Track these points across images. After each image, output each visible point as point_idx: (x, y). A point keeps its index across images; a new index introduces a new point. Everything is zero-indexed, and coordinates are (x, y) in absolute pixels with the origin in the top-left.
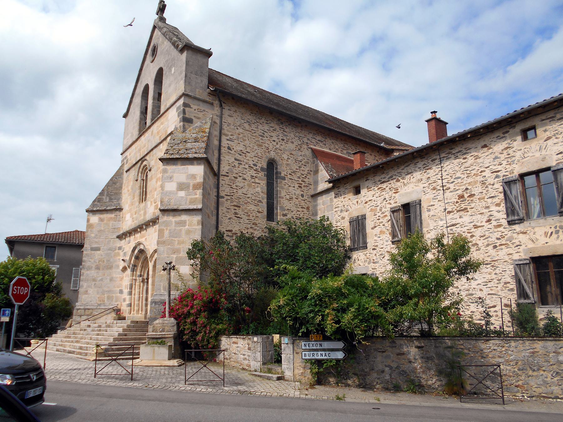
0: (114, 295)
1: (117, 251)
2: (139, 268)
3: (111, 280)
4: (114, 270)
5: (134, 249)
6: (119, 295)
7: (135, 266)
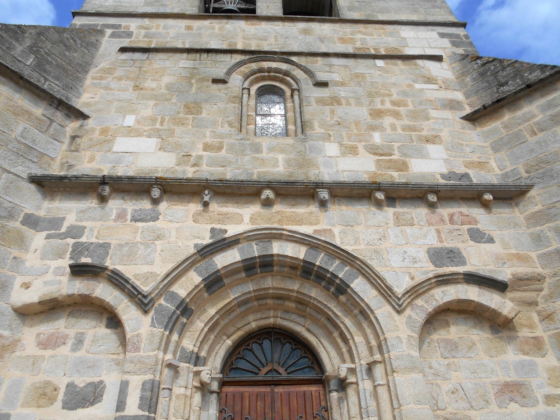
1: (16, 224)
2: (199, 325)
5: (348, 258)
7: (185, 310)
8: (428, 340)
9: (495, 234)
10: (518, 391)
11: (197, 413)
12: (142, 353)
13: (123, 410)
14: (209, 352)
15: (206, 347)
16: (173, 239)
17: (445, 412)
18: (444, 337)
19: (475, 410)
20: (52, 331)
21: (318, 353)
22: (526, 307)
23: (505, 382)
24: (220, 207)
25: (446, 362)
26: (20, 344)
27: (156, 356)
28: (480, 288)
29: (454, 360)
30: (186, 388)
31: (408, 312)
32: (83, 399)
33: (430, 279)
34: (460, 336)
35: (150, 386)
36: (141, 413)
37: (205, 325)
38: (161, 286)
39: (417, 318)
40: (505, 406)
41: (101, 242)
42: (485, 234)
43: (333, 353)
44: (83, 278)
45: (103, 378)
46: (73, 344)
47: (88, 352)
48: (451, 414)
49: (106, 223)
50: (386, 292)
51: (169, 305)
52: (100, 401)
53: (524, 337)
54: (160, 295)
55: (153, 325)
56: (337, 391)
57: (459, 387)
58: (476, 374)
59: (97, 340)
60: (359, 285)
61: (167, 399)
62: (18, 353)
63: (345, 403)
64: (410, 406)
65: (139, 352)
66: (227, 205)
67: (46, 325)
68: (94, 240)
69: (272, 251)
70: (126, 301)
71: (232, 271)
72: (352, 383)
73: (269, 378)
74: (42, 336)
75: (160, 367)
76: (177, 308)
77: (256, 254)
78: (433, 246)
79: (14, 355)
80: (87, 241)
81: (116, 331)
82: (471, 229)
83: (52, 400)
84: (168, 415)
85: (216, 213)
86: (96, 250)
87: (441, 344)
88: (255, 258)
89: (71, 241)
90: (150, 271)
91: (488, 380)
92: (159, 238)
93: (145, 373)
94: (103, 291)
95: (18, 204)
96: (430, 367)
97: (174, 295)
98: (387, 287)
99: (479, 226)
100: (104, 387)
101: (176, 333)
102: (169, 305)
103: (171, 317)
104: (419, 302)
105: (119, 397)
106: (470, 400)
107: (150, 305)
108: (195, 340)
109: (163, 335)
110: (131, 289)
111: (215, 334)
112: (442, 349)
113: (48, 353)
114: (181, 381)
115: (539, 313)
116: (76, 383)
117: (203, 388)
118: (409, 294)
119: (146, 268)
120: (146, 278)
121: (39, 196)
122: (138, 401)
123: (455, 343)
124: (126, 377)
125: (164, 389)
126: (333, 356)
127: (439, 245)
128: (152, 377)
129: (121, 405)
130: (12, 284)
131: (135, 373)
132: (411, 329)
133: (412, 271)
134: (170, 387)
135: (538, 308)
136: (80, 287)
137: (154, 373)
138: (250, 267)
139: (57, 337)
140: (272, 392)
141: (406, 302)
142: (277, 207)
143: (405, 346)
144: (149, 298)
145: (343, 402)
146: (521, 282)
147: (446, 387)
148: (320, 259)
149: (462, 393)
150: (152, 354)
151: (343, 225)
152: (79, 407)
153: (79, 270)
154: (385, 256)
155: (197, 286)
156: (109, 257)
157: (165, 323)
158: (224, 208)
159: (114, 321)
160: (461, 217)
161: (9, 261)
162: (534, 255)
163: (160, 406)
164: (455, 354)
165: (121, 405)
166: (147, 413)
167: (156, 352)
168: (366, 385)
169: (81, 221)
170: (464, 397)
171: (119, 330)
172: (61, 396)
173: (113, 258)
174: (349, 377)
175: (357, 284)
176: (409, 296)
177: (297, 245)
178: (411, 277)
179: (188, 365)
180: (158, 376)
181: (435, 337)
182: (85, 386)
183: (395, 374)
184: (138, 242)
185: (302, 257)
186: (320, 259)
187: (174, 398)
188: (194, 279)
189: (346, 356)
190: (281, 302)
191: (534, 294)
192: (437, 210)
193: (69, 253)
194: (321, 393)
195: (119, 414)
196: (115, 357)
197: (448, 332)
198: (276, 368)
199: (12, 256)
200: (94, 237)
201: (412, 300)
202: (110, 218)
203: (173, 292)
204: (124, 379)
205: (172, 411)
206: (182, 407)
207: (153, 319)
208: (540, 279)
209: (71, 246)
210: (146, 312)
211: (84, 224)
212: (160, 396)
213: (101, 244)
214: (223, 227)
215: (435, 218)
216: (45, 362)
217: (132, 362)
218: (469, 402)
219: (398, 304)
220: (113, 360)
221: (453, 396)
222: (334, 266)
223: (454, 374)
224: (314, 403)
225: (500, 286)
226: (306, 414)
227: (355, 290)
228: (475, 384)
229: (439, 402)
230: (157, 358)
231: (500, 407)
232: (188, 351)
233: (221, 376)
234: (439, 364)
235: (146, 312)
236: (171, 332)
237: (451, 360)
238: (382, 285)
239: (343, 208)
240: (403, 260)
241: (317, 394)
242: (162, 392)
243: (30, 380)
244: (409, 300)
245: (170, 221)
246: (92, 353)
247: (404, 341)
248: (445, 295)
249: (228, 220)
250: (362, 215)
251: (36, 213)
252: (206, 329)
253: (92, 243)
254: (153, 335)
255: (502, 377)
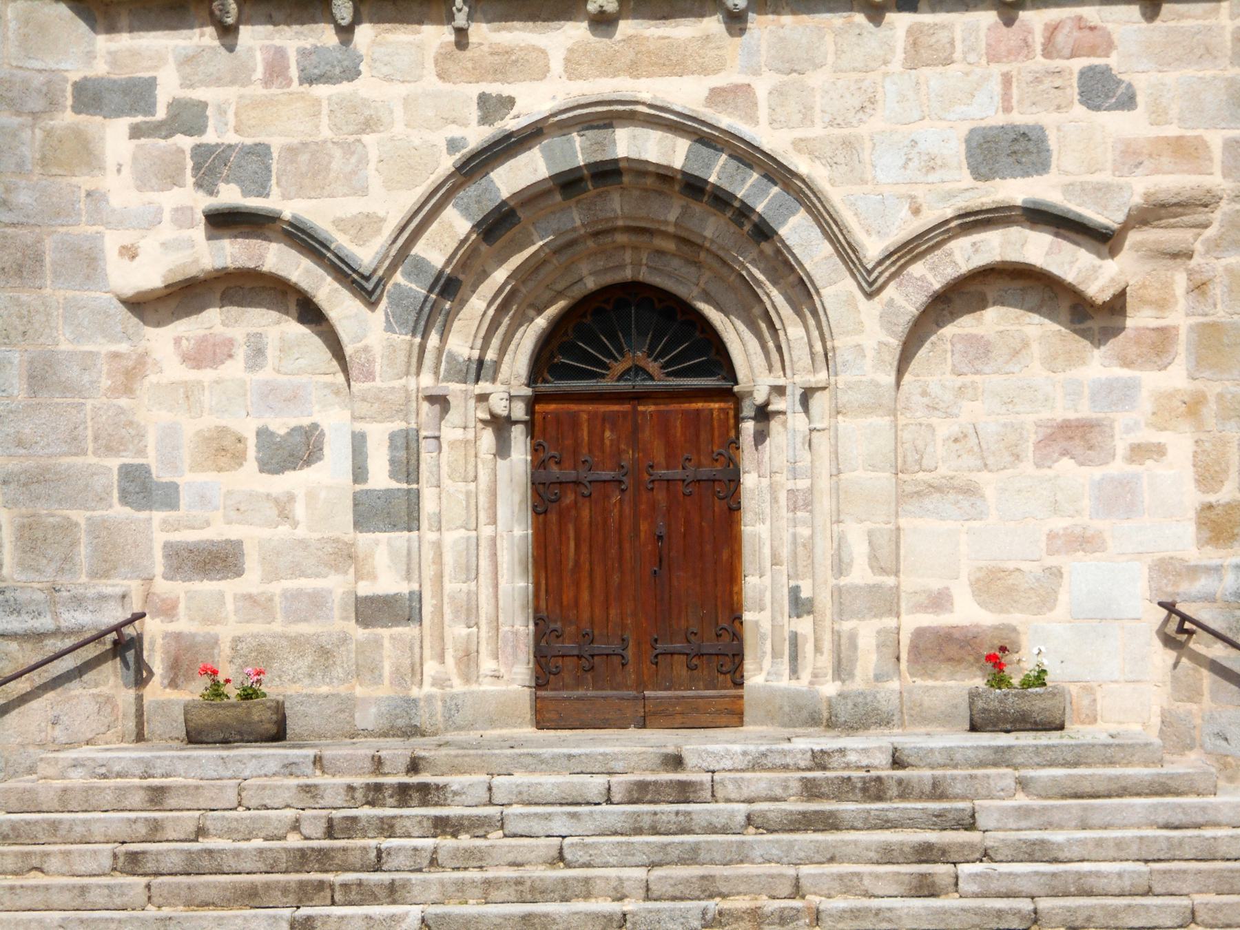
0: (79, 516)
1: (67, 118)
2: (478, 304)
3: (41, 376)
4: (55, 292)
5: (776, 172)
6: (119, 511)
7: (449, 287)
8: (933, 338)
9: (1143, 80)
10: (1083, 437)
11: (491, 465)
12: (378, 383)
13: (365, 480)
14: (502, 351)
15: (495, 342)
16: (399, 128)
17: (933, 474)
18: (967, 330)
19: (990, 471)
20: (201, 332)
22: (1165, 261)
23: (1064, 421)
24: (495, 31)
25: (959, 381)
26: (150, 360)
27: (405, 389)
28: (1057, 235)
29: (977, 378)
30: (465, 428)
31: (890, 291)
32: (292, 455)
33: (946, 222)
34: (1001, 328)
35: (404, 441)
36: (394, 485)
37: (489, 306)
38: (393, 252)
39: (904, 304)
40: (1049, 463)
41: (249, 141)
42: (1119, 82)
44: (235, 232)
45: (316, 418)
46: (248, 356)
47: (279, 372)
48: (944, 477)
49: (247, 91)
50: (847, 252)
51: (414, 286)
52: (319, 459)
53: (1137, 329)
54: (392, 268)
55: (389, 328)
56: (754, 418)
57: (971, 431)
58: (1011, 406)
59: (289, 348)
60: (797, 231)
61: (435, 454)
62: (153, 378)
64: (856, 473)
65: (374, 380)
66: (509, 24)
67: (185, 321)
68: (232, 138)
69: (614, 151)
70: (329, 279)
71: (532, 196)
73: (624, 386)
74: (184, 342)
75: (414, 404)
76: (431, 290)
77: (582, 163)
78: (983, 124)
79: (146, 382)
80: (220, 141)
81: (319, 328)
82: (1092, 68)
83: (239, 459)
84: (439, 480)
85: (485, 48)
86: (243, 163)
87: (959, 346)
88: (579, 168)
89: (185, 142)
90: (365, 211)
91: (1031, 418)
92: (369, 125)
93: (390, 418)
94: (277, 258)
95: (54, 67)
96: (924, 394)
97: (420, 266)
98: (849, 243)
99: (1113, 61)
100: (322, 434)
101: (433, 332)
102: (414, 286)
103: (422, 309)
104: (917, 269)
105: (354, 459)
106: (985, 454)
107: (378, 291)
108: (472, 338)
109: (412, 345)
110: (333, 258)
111: (511, 314)
112: (956, 356)
113: (207, 375)
114: (454, 416)
115: (1190, 273)
116: (271, 428)
117: (500, 425)
118: (895, 257)
119: (363, 207)
120: (364, 225)
121: (82, 27)
122: (386, 467)
123: (988, 343)
124: (360, 426)
125: (425, 438)
127: (1000, 119)
128: (403, 425)
129: (360, 473)
130: (102, 250)
131: (373, 419)
132: (888, 330)
133: (920, 192)
134: (437, 434)
135: (1193, 263)
136: (232, 252)
137: (406, 419)
138: (568, 184)
139: (214, 345)
140: (635, 411)
141: (887, 274)
142: (626, 27)
143: (868, 363)
144: (375, 279)
146: (1163, 211)
147: (945, 428)
148: (717, 168)
149: (973, 441)
150: (397, 383)
151: (779, 71)
152: (288, 469)
153: (223, 222)
154: (866, 156)
155: (463, 242)
156: (274, 181)
157: (412, 324)
158: (503, 33)
159: (310, 312)
160: (1076, 34)
161: (82, 205)
162: (1215, 139)
163: (423, 467)
164: (980, 367)
165: (360, 473)
166: (405, 486)
167: (403, 381)
168: (798, 421)
169: (191, 86)
170: (976, 449)
171: (324, 327)
172: (252, 452)
173: (283, 183)
175: (794, 229)
176: (894, 263)
177: (670, 135)
178: (914, 206)
179: (462, 386)
180: (413, 421)
181: (949, 331)
182: (288, 434)
183: (840, 417)
184: (325, 142)
185: (678, 164)
186: (717, 168)
187: (445, 446)
188: (456, 224)
189: (778, 365)
190: (644, 238)
191: (1188, 234)
192: (1021, 13)
193: (189, 172)
195: (359, 487)
196: (329, 379)
197: (980, 321)
198: (642, 364)
199: (83, 194)
200: (232, 131)
201: (903, 267)
202: (253, 78)
203: (416, 256)
204: (357, 430)
205: (445, 470)
206: (462, 462)
207: (387, 315)
208: (1206, 202)
209: (188, 155)
210: (372, 305)
211: (200, 94)
212: (422, 451)
213: (250, 147)
214: (506, 90)
215: (1011, 36)
216: (207, 393)
217: (364, 400)
218: (983, 458)
219: (867, 281)
220: (326, 385)
221: (958, 446)
222: (745, 185)
223: (966, 405)
225: (1102, 239)
227: (788, 243)
228: (1005, 425)
229: (926, 456)
230: (407, 390)
231: (1038, 466)
232: (461, 360)
233: (528, 391)
234: (943, 386)
235: (372, 305)
236: (425, 336)
237: (970, 378)
238: (841, 238)
239: (787, 19)
240: (905, 167)
242: (423, 443)
243: (191, 427)
244: (893, 269)
245: (388, 79)
246: (286, 374)
247: (870, 354)
248: (976, 251)
249: (514, 70)
250: (829, 38)
251: (90, 73)
252: (491, 312)
253: (230, 146)
254: (392, 347)
255: (1062, 411)
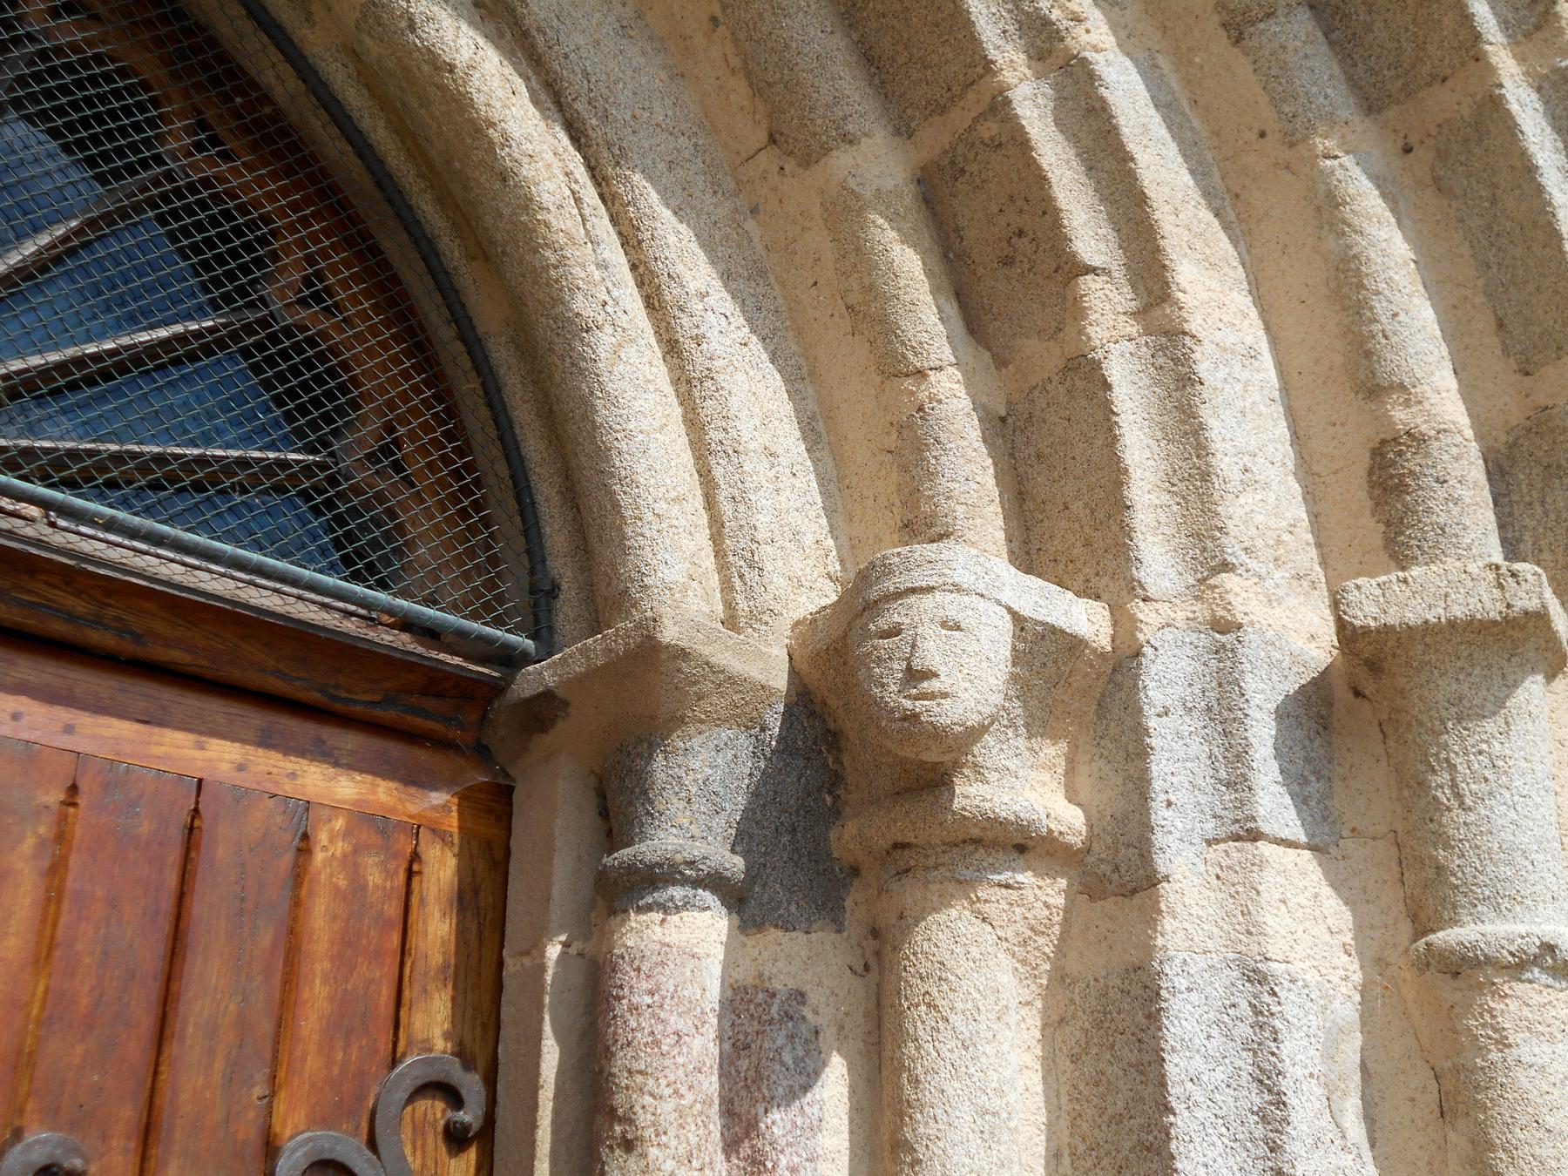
21: (573, 329)
43: (756, 397)
63: (835, 1084)
72: (1021, 844)
126: (747, 429)
145: (807, 1078)
174: (990, 751)
194: (442, 868)
224: (317, 996)
226: (148, 1132)
241: (378, 876)
